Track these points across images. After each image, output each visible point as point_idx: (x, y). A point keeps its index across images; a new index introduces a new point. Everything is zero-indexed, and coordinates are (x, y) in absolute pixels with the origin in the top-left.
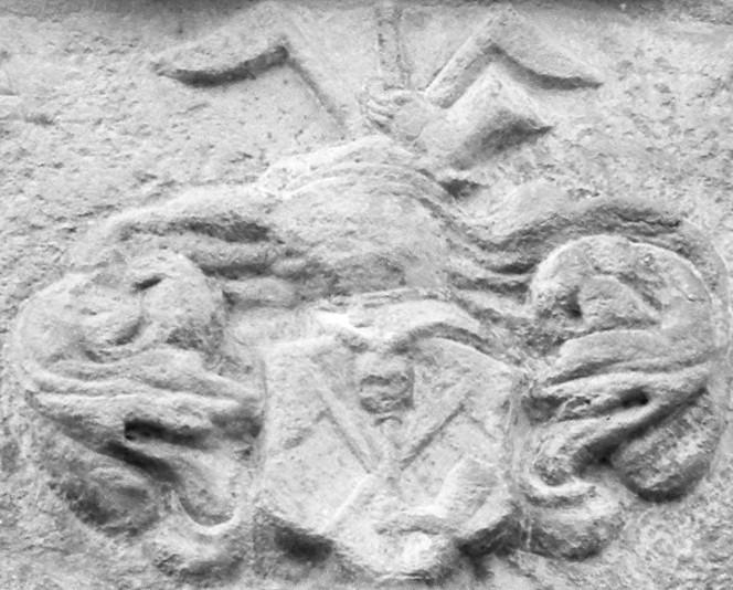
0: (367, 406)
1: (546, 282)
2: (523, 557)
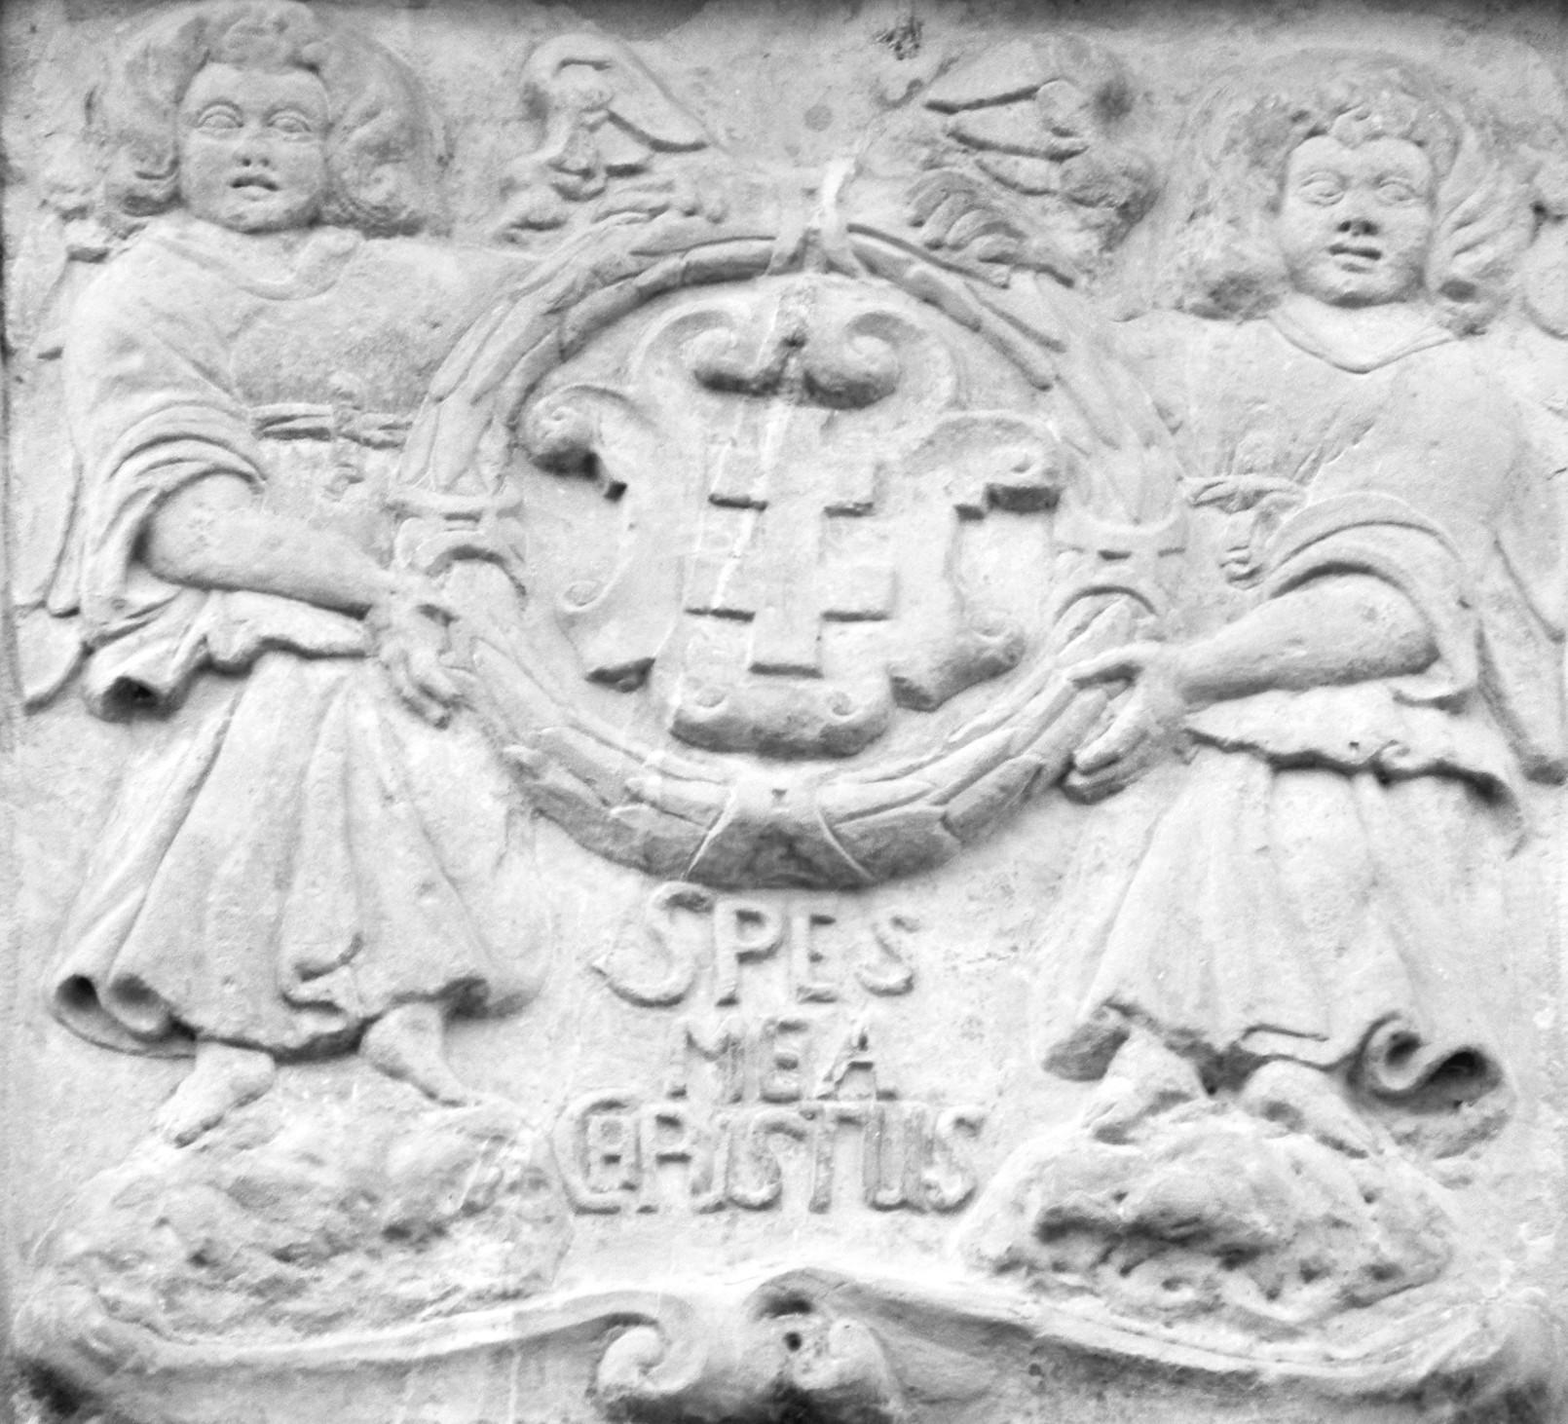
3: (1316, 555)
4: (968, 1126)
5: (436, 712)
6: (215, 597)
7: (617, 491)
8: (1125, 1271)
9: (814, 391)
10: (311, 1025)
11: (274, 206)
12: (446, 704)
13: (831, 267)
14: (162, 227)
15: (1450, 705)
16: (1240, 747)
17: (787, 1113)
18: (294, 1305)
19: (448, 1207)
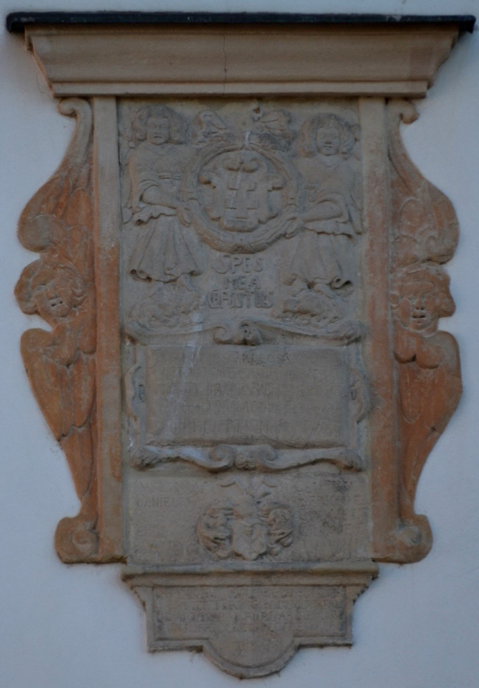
0: (247, 535)
1: (271, 516)
2: (268, 555)
3: (323, 198)
4: (271, 293)
5: (188, 225)
6: (153, 206)
7: (215, 187)
8: (296, 318)
9: (244, 170)
10: (169, 278)
11: (161, 140)
12: (189, 224)
13: (247, 149)
14: (143, 144)
15: (345, 223)
16: (312, 230)
17: (243, 292)
18: (168, 324)
19: (191, 308)
